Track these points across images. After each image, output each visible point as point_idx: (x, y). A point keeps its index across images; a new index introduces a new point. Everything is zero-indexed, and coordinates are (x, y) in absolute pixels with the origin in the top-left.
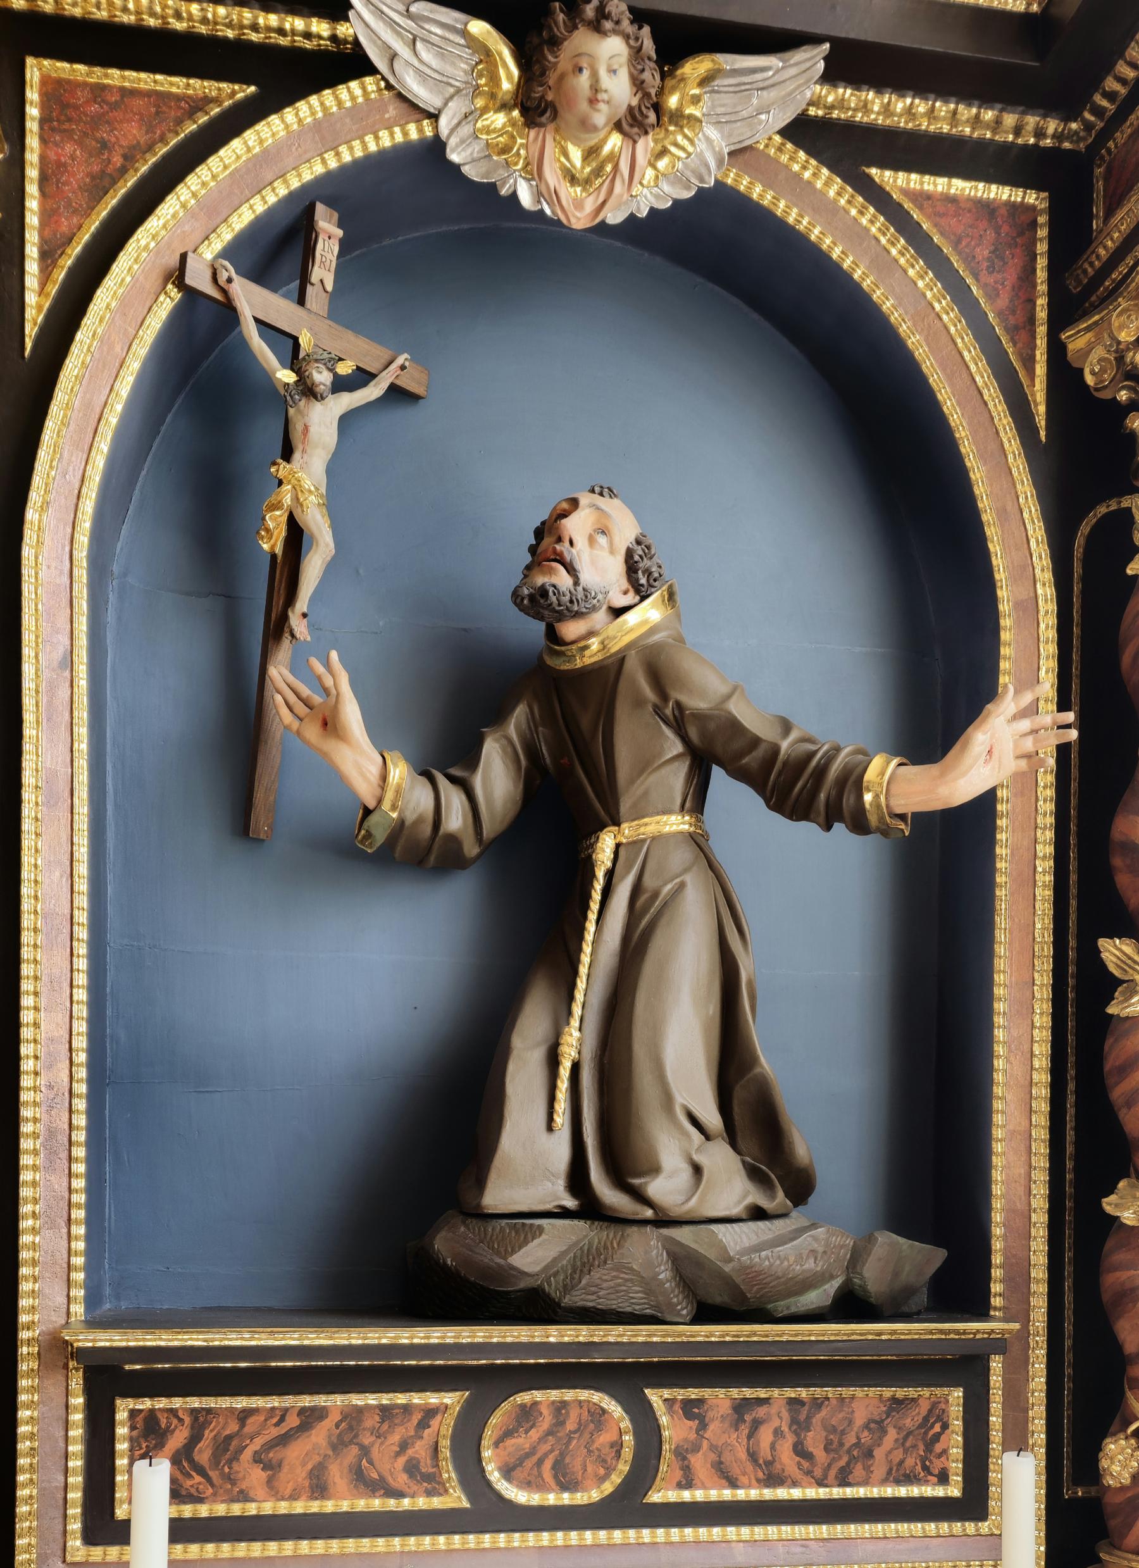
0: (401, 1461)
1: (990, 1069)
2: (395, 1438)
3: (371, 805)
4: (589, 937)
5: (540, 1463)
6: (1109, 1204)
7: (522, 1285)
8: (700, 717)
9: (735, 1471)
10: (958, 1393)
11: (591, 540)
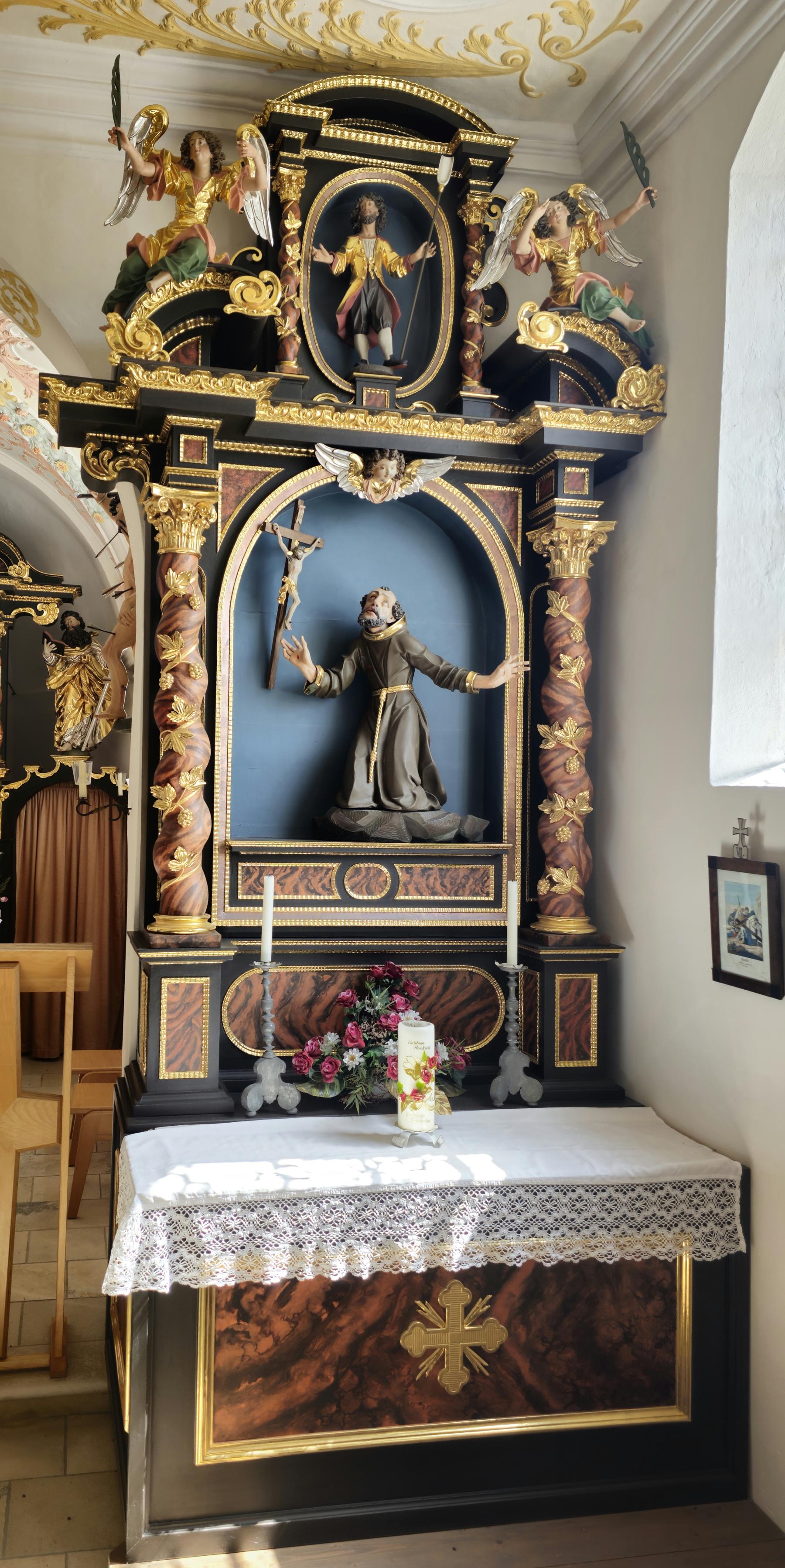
0: (320, 884)
1: (503, 763)
2: (318, 877)
3: (311, 681)
4: (379, 722)
5: (362, 886)
6: (540, 807)
7: (359, 830)
8: (415, 658)
9: (422, 891)
10: (493, 867)
11: (382, 604)
